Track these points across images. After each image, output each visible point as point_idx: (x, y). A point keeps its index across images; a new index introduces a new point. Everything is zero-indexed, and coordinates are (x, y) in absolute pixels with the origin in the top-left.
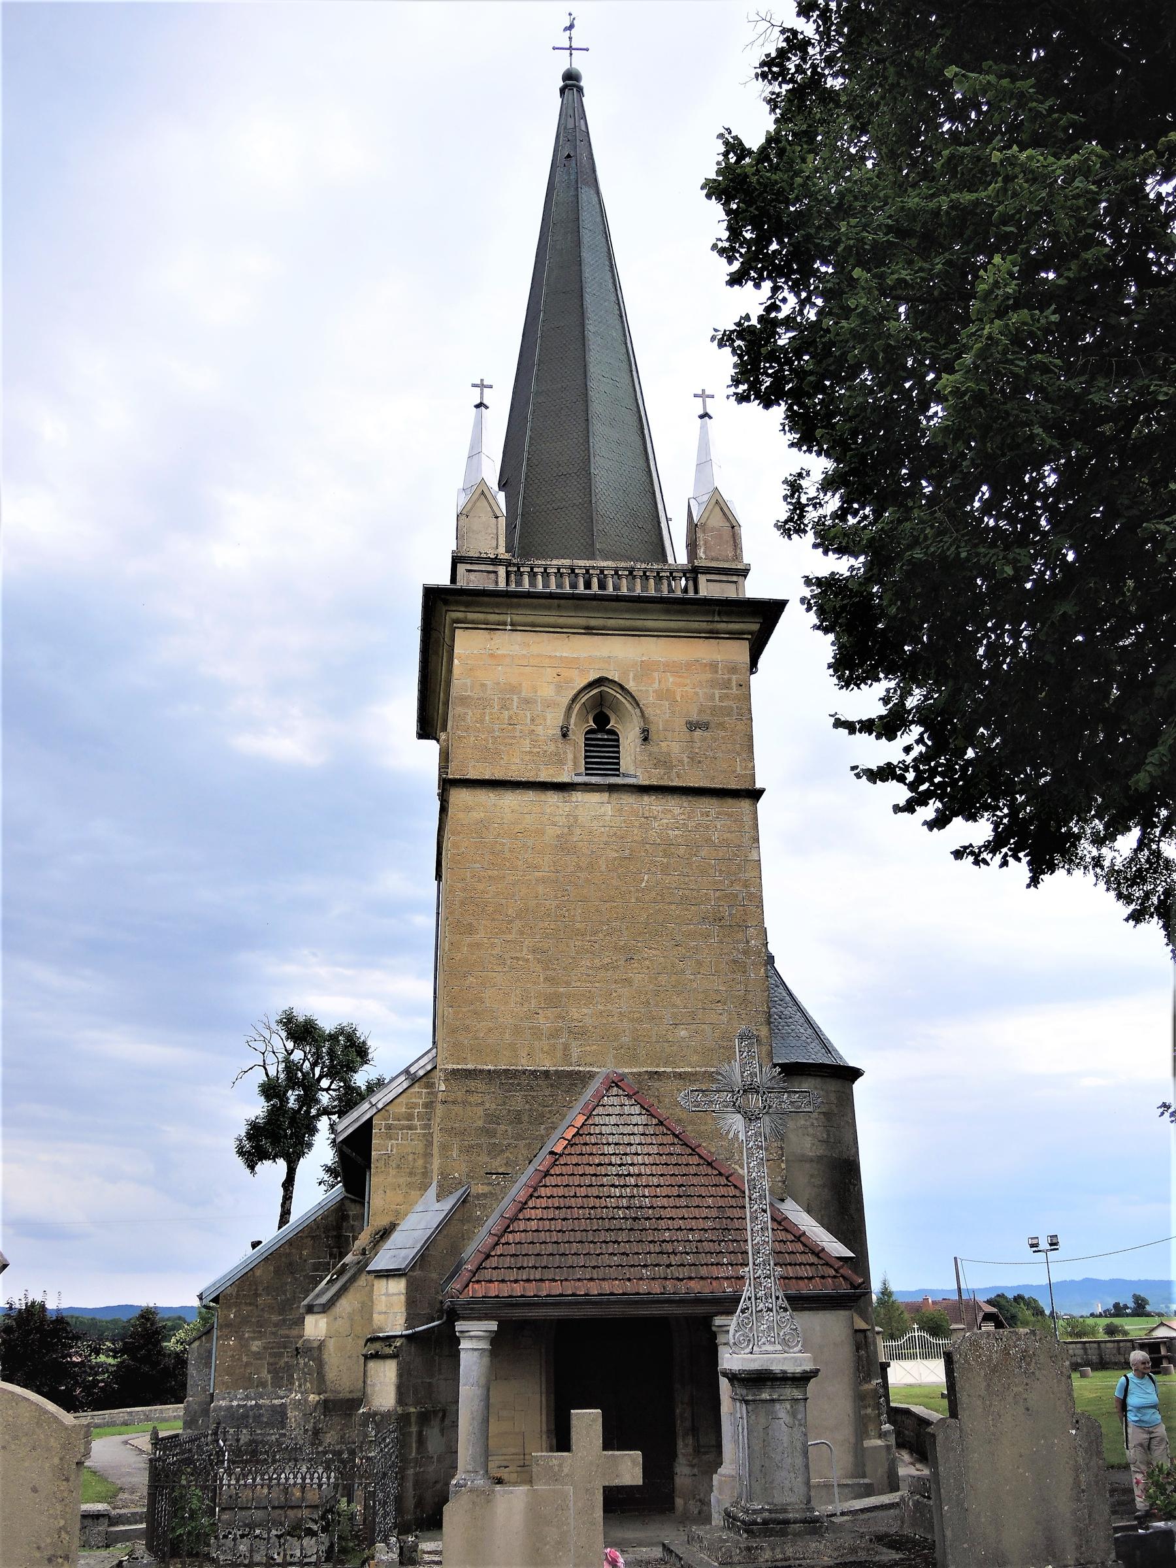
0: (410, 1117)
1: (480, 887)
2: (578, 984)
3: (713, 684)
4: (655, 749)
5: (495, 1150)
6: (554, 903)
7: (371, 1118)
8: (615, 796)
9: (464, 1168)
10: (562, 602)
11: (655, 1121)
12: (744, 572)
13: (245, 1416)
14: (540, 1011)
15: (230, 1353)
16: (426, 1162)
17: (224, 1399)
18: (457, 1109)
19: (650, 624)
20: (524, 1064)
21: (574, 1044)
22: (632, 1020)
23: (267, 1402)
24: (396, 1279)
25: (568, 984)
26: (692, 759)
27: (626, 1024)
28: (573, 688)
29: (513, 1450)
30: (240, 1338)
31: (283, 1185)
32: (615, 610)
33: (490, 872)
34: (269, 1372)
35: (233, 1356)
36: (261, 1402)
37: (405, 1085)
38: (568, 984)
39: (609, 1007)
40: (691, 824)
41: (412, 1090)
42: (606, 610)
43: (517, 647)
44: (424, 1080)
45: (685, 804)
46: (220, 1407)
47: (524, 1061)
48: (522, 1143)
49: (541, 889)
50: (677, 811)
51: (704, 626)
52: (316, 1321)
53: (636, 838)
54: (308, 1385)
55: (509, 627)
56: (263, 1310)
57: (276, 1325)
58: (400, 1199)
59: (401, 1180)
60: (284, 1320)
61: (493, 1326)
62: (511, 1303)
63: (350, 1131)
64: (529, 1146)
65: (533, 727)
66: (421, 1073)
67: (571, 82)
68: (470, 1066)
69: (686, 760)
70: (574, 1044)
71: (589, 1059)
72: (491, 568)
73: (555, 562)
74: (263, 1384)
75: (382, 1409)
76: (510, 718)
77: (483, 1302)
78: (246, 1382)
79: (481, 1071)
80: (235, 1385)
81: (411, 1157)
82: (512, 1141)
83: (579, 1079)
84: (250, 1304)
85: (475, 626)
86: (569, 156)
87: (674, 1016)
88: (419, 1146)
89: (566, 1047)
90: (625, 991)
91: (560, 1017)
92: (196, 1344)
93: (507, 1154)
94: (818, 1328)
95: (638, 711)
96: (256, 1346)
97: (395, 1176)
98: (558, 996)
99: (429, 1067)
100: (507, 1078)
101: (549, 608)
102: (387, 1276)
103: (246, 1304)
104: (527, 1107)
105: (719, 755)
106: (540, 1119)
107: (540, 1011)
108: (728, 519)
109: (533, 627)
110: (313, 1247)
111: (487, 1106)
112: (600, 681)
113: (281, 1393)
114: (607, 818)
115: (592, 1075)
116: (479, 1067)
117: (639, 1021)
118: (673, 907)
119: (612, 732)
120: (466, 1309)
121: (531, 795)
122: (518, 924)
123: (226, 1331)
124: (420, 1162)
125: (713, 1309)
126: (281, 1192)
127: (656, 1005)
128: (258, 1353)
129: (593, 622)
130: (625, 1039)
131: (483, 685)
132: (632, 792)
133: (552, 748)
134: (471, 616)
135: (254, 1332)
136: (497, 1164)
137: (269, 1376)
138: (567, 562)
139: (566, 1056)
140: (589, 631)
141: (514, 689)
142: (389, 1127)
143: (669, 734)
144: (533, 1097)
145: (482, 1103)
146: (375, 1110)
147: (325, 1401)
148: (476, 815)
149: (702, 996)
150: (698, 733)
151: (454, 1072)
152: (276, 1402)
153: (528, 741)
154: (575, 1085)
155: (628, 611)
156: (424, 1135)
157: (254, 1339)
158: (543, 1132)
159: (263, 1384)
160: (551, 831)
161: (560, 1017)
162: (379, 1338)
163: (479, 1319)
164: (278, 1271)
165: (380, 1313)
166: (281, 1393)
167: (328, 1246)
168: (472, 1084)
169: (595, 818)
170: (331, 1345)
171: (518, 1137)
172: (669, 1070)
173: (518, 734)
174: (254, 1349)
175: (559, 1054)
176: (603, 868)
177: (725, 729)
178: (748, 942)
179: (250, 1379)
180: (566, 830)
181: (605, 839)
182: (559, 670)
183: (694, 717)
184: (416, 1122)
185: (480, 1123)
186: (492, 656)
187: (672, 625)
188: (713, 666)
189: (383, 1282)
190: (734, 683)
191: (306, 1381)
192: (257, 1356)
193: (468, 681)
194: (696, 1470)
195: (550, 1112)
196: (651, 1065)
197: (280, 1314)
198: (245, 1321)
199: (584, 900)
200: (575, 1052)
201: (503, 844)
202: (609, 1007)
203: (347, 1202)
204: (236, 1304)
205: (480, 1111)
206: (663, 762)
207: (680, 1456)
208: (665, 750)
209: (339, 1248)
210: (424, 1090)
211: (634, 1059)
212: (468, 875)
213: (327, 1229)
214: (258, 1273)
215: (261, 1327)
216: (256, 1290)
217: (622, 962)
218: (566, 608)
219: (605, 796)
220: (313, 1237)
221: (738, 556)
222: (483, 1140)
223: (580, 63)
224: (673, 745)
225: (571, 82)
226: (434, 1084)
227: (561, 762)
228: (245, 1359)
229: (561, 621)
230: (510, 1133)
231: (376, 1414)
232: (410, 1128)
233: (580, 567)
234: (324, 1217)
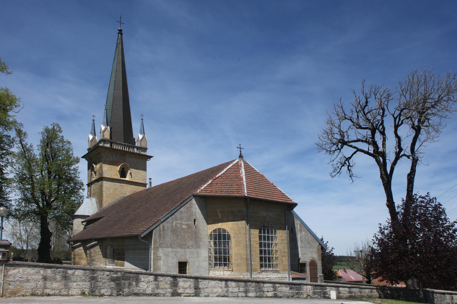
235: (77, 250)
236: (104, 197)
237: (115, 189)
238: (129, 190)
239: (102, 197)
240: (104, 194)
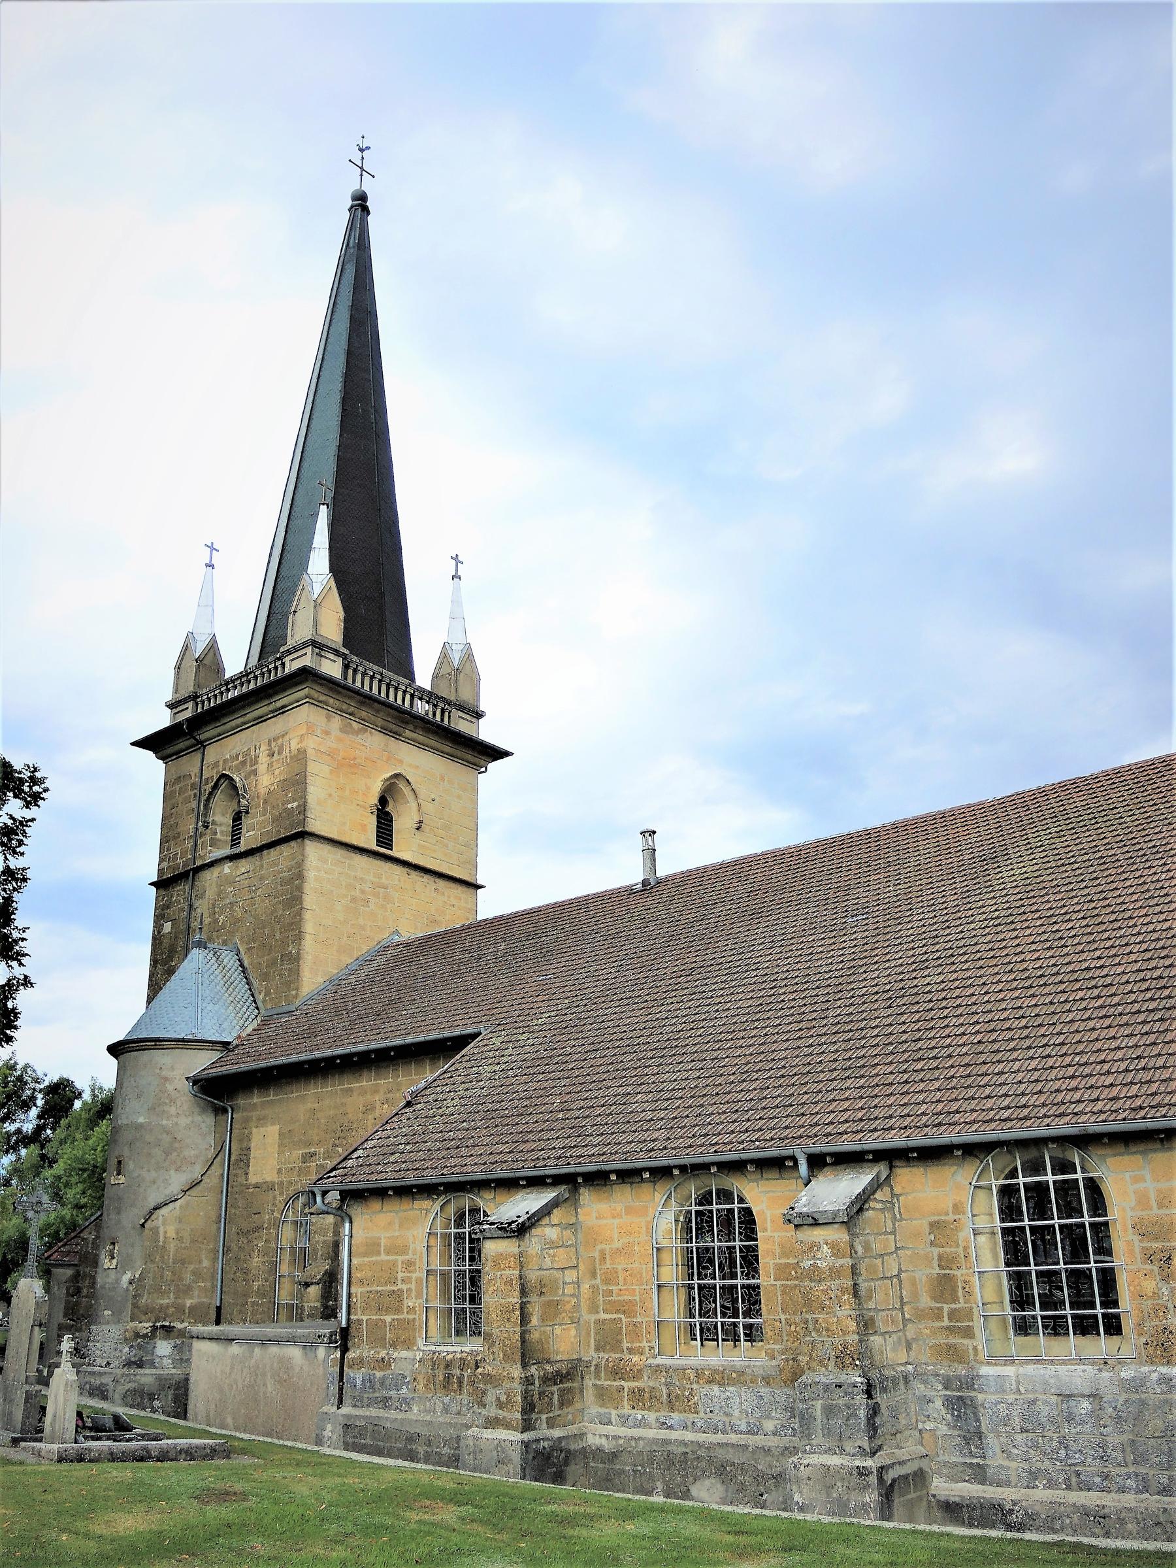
12: (479, 715)
67: (360, 204)
112: (397, 776)
119: (388, 814)
225: (360, 204)
235: (598, 1210)
236: (308, 944)
237: (354, 899)
238: (415, 912)
239: (298, 938)
240: (309, 927)
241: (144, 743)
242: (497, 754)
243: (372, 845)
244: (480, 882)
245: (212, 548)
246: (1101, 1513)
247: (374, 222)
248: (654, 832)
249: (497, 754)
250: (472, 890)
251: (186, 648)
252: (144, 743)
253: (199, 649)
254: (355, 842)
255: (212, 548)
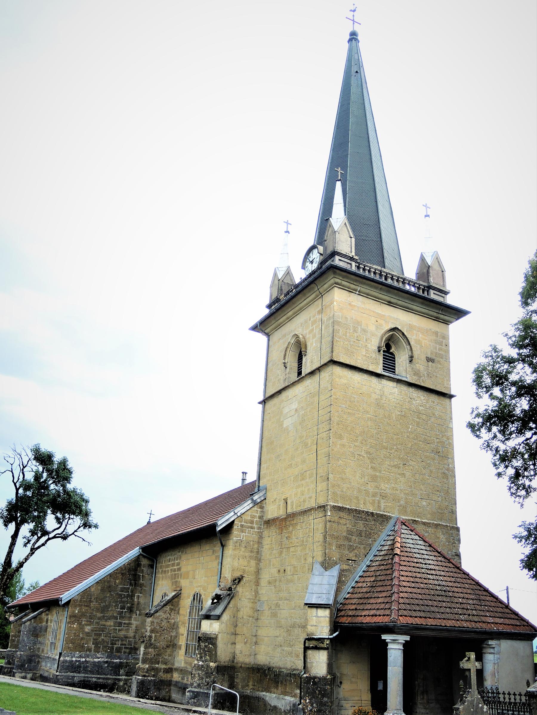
0: (252, 522)
1: (345, 417)
2: (384, 472)
3: (436, 342)
4: (414, 367)
5: (351, 548)
6: (375, 431)
7: (234, 520)
8: (399, 385)
9: (338, 556)
10: (384, 287)
11: (427, 544)
12: (446, 293)
13: (79, 667)
14: (369, 483)
15: (73, 632)
16: (259, 547)
17: (68, 656)
18: (335, 525)
19: (414, 307)
20: (362, 507)
21: (382, 501)
22: (405, 494)
23: (91, 660)
24: (323, 609)
25: (380, 472)
26: (428, 375)
27: (403, 495)
28: (382, 329)
29: (356, 698)
30: (80, 624)
31: (12, 537)
32: (403, 297)
33: (349, 410)
34: (93, 644)
35: (75, 633)
36: (88, 659)
37: (251, 505)
38: (380, 472)
39: (396, 486)
40: (428, 405)
41: (253, 509)
42: (399, 296)
43: (360, 303)
44: (259, 504)
45: (425, 395)
46: (66, 661)
47: (362, 506)
48: (362, 546)
49: (369, 423)
50: (422, 398)
51: (435, 314)
52: (211, 624)
53: (407, 407)
54: (208, 657)
55: (357, 293)
56: (93, 610)
57: (99, 619)
58: (246, 563)
59: (247, 554)
60: (104, 616)
61: (408, 638)
62: (417, 628)
63: (224, 525)
64: (365, 548)
65: (366, 344)
66: (259, 501)
67: (353, 37)
68: (339, 505)
69: (426, 375)
70: (382, 501)
71: (388, 510)
72: (349, 261)
73: (374, 266)
74: (90, 650)
75: (319, 675)
76: (357, 337)
77: (408, 626)
78: (81, 648)
79: (346, 508)
80: (75, 649)
81: (252, 543)
82: (357, 545)
83: (384, 519)
84: (87, 606)
85: (343, 288)
86: (357, 72)
87: (421, 494)
88: (256, 537)
89: (379, 502)
90: (402, 479)
91: (377, 487)
92: (28, 623)
93: (356, 551)
94: (522, 648)
95: (408, 347)
96: (87, 629)
97: (244, 552)
98: (376, 477)
99: (262, 499)
100: (356, 513)
101: (376, 288)
102: (317, 607)
103: (85, 606)
104: (364, 529)
105: (438, 375)
106: (369, 535)
107: (369, 483)
108: (441, 267)
109: (367, 296)
110: (122, 578)
111: (348, 526)
112: (395, 329)
113: (98, 655)
114: (396, 395)
115: (390, 518)
116: (345, 506)
117: (408, 494)
118: (421, 443)
119: (392, 354)
120: (399, 629)
121: (365, 376)
122: (360, 438)
123: (73, 619)
124: (256, 546)
125: (488, 637)
126: (10, 540)
127: (415, 488)
128: (89, 633)
129: (393, 300)
130: (402, 502)
131: (346, 318)
132: (406, 385)
133: (374, 356)
134: (344, 283)
135: (87, 621)
136: (352, 556)
137: (93, 646)
138: (379, 268)
139: (379, 507)
140: (390, 303)
141: (359, 323)
142: (242, 526)
143: (420, 361)
144: (367, 524)
145: (346, 524)
146: (236, 516)
147: (218, 666)
148: (344, 381)
149: (431, 487)
150: (430, 363)
151: (334, 507)
152: (96, 660)
153: (364, 350)
154: (384, 521)
155: (407, 299)
156: (258, 532)
157: (87, 625)
158: (371, 542)
159: (90, 650)
160: (374, 396)
161: (377, 487)
162: (314, 639)
163: (401, 634)
164: (103, 590)
165: (312, 626)
166: (98, 655)
167: (130, 579)
168: (342, 514)
169: (391, 394)
170: (220, 637)
171: (361, 543)
172: (419, 520)
173: (360, 345)
174: (86, 630)
175: (376, 505)
176: (394, 418)
177: (440, 364)
178: (449, 465)
179: (83, 647)
180: (380, 397)
181: (394, 404)
182: (377, 319)
183: (429, 356)
184: (255, 525)
185: (345, 534)
186: (350, 304)
187: (423, 310)
188: (436, 333)
189: (314, 610)
190: (444, 344)
191: (206, 655)
192: (88, 634)
193: (340, 314)
194: (428, 711)
195: (374, 533)
196: (412, 516)
197: (102, 613)
198: (83, 615)
199: (387, 432)
200: (382, 505)
201: (355, 398)
202: (396, 486)
203: (141, 557)
204: (80, 606)
205: (345, 529)
206: (417, 373)
207: (419, 704)
208: (418, 368)
209: (134, 580)
210: (259, 510)
211: (405, 513)
212: (340, 410)
213: (129, 570)
214: (93, 589)
215: (91, 619)
216: (91, 599)
217: (401, 465)
218: (384, 291)
219: (394, 384)
220: (122, 574)
221: (444, 285)
222: (346, 543)
223: (357, 28)
224: (420, 365)
225: (353, 37)
226: (264, 507)
227: (378, 364)
228: (81, 636)
229: (381, 296)
230: (357, 540)
231: (315, 678)
232: (252, 528)
233: (384, 272)
234: (129, 564)
241: (255, 328)
242: (458, 313)
243: (379, 370)
244: (453, 393)
245: (287, 223)
246: (384, 348)
247: (362, 45)
248: (246, 473)
249: (458, 313)
250: (447, 400)
251: (275, 274)
252: (255, 328)
253: (280, 275)
254: (348, 362)
255: (287, 223)
